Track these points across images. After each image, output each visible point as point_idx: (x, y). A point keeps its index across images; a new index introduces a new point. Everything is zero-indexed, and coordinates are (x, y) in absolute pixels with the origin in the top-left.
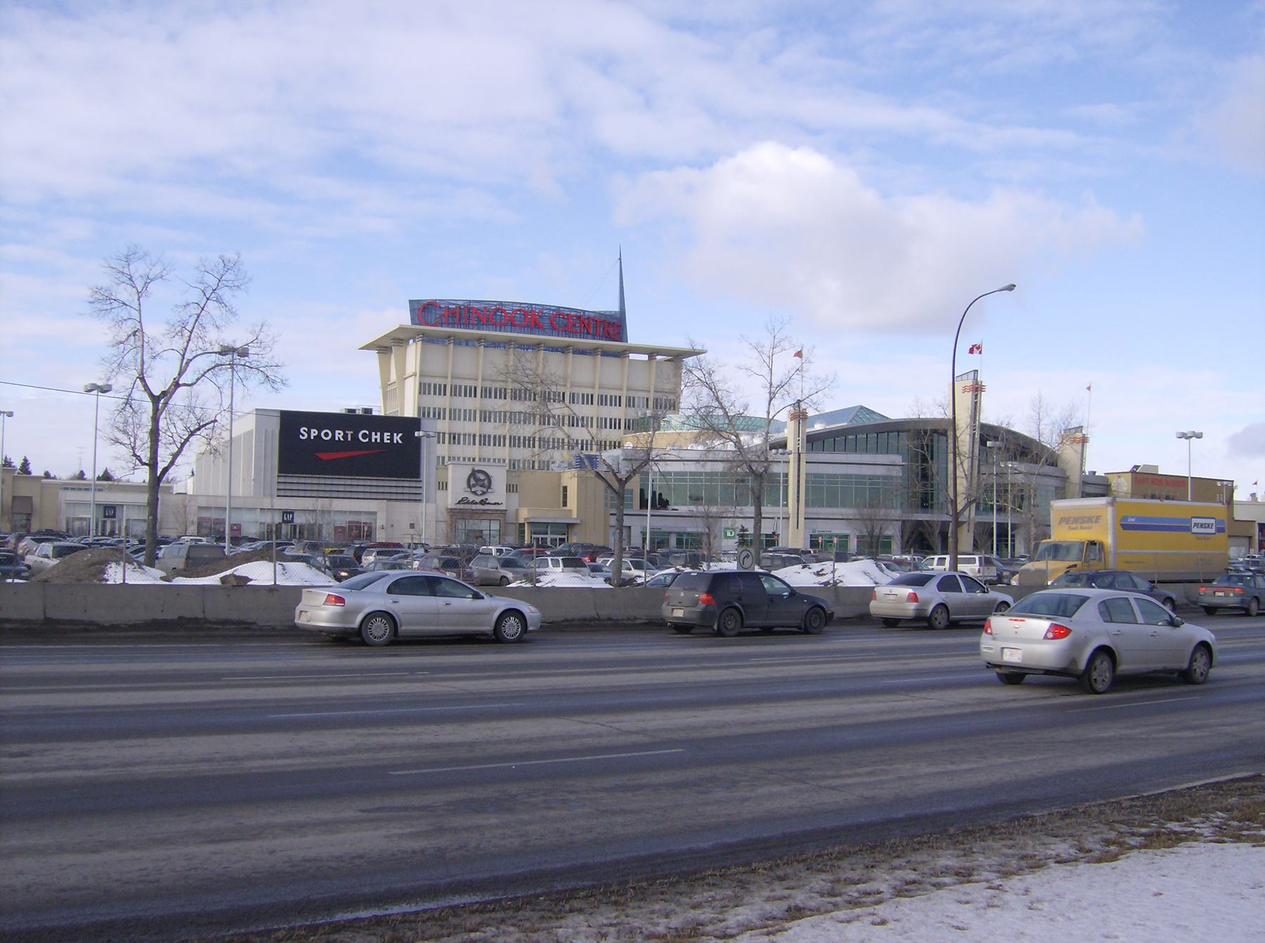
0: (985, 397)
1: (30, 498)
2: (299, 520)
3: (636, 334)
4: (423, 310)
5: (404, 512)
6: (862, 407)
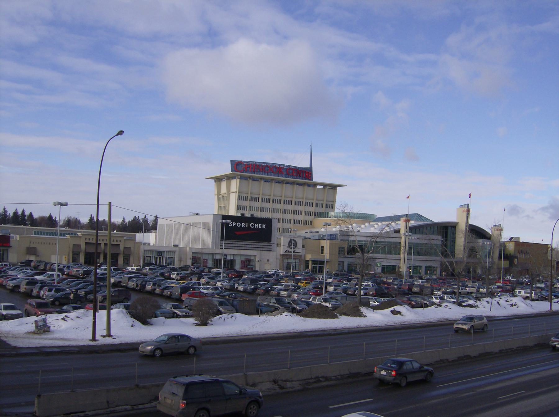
0: (471, 215)
1: (130, 248)
2: (229, 258)
3: (316, 178)
4: (236, 165)
5: (266, 255)
6: (418, 214)
